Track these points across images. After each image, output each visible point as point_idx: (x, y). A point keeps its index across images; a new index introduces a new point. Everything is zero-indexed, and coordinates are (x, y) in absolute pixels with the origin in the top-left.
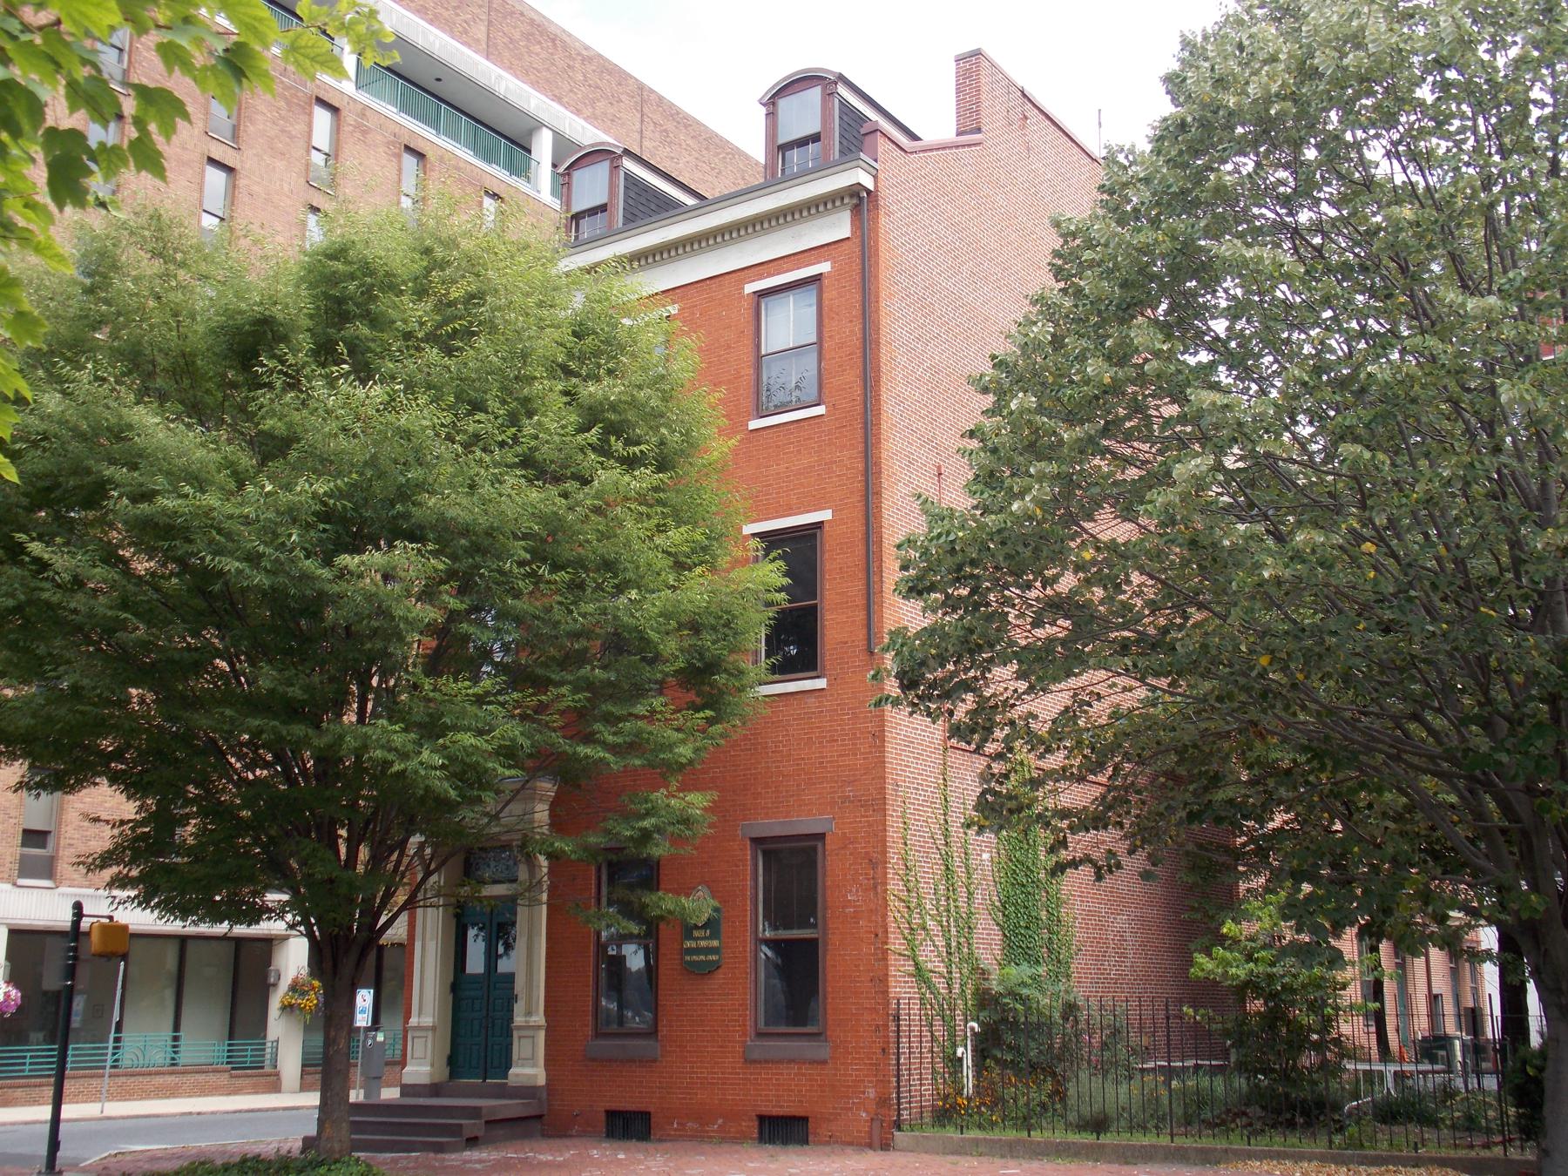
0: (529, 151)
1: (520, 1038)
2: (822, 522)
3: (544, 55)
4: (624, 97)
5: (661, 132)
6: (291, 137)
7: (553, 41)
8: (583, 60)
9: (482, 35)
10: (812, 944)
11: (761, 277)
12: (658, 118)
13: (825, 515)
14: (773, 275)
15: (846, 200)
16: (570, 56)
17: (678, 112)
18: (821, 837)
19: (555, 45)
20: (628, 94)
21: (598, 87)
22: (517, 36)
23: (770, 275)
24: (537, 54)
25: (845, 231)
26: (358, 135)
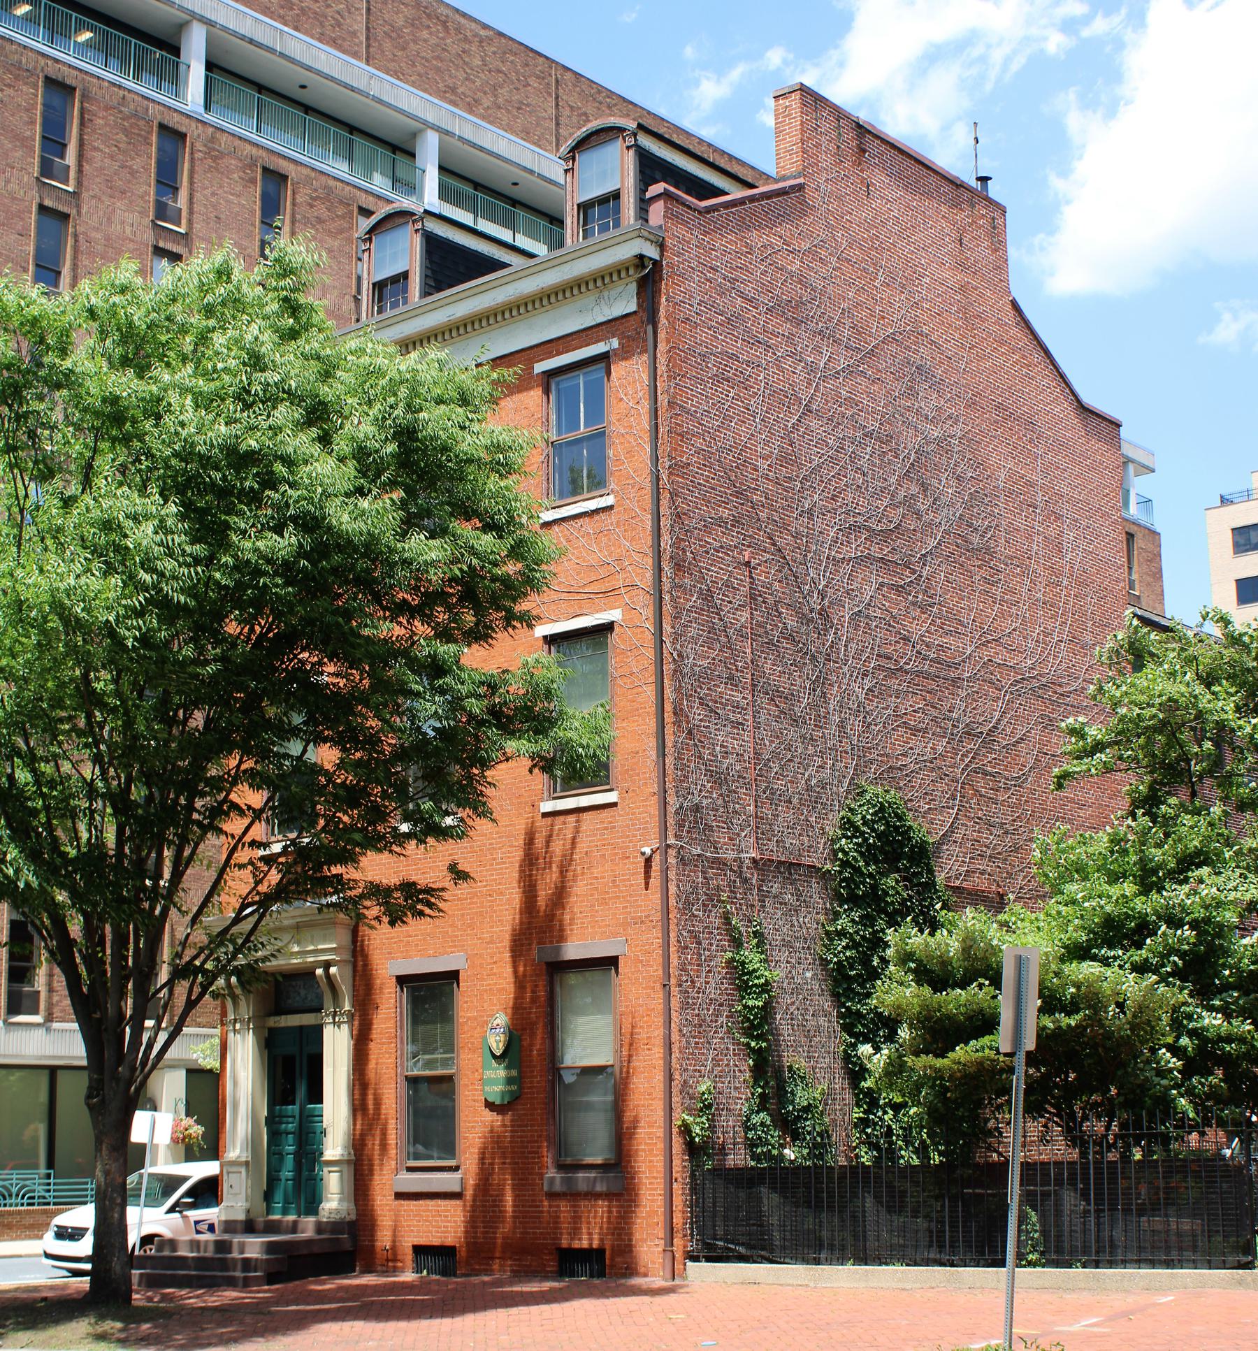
0: (413, 155)
1: (228, 1173)
2: (613, 623)
3: (434, 41)
4: (532, 81)
5: (579, 115)
6: (133, 173)
7: (444, 23)
8: (481, 42)
9: (358, 23)
10: (449, 1079)
11: (550, 356)
12: (575, 100)
13: (614, 615)
14: (562, 353)
15: (631, 271)
16: (466, 39)
17: (601, 89)
18: (454, 976)
19: (446, 29)
20: (538, 77)
21: (500, 72)
22: (400, 22)
23: (559, 353)
24: (425, 41)
25: (632, 307)
26: (210, 162)
